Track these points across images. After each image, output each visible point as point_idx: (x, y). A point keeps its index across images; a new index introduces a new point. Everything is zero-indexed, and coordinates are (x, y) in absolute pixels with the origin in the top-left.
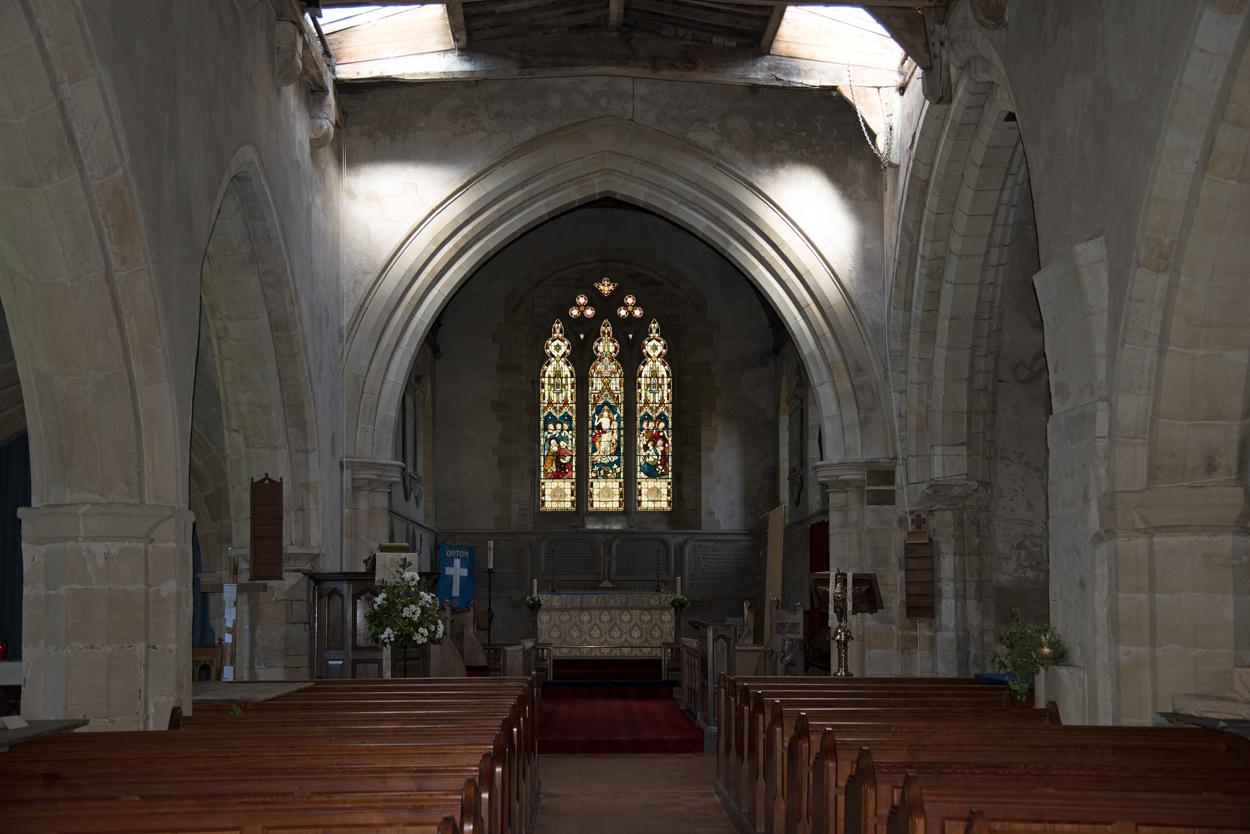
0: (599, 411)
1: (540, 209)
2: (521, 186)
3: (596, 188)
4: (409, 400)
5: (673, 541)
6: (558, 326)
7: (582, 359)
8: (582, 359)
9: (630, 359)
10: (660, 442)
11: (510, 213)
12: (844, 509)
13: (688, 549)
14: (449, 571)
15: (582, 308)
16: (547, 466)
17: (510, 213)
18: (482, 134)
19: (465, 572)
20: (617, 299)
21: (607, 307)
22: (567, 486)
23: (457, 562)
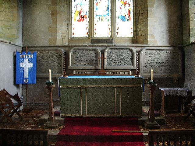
5: (135, 50)
10: (127, 5)
16: (75, 17)
23: (27, 60)
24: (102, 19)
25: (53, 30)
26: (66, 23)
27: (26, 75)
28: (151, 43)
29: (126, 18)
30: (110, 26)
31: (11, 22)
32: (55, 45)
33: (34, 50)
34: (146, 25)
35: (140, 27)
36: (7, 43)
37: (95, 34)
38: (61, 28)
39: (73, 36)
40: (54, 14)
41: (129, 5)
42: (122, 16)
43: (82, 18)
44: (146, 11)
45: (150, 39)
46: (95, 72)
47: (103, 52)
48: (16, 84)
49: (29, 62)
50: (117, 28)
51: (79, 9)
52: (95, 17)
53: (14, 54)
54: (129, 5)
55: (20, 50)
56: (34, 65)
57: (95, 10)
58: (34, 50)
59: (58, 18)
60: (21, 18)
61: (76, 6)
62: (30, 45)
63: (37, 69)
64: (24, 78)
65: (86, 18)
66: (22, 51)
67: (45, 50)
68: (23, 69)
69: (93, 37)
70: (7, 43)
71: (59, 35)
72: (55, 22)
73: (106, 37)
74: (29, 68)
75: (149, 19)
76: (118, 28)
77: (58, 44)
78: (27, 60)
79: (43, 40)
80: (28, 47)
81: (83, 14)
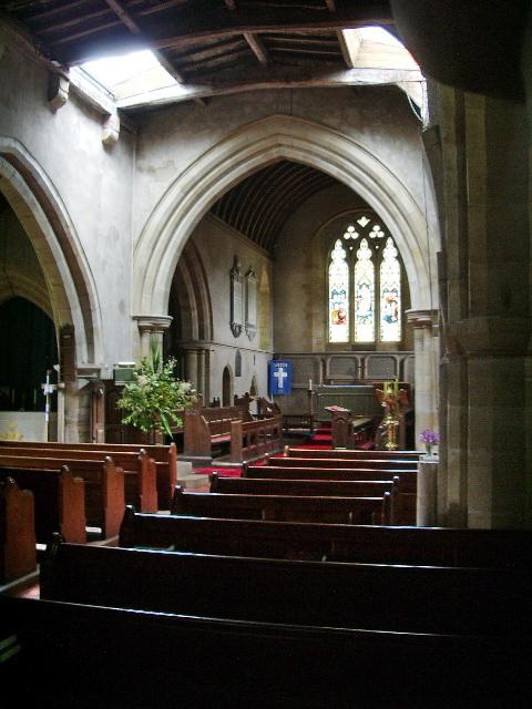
0: (361, 287)
1: (243, 169)
2: (230, 157)
3: (275, 154)
4: (186, 276)
5: (398, 359)
6: (339, 243)
7: (351, 260)
8: (351, 260)
9: (377, 259)
11: (226, 172)
12: (422, 340)
13: (366, 360)
14: (276, 374)
15: (351, 233)
16: (333, 318)
17: (226, 172)
18: (208, 131)
19: (286, 375)
20: (369, 228)
21: (364, 232)
22: (345, 327)
25: (308, 335)
26: (322, 325)
38: (317, 333)
40: (309, 316)
43: (341, 319)
46: (355, 382)
47: (363, 360)
71: (315, 341)
72: (310, 326)
77: (314, 352)
79: (297, 347)
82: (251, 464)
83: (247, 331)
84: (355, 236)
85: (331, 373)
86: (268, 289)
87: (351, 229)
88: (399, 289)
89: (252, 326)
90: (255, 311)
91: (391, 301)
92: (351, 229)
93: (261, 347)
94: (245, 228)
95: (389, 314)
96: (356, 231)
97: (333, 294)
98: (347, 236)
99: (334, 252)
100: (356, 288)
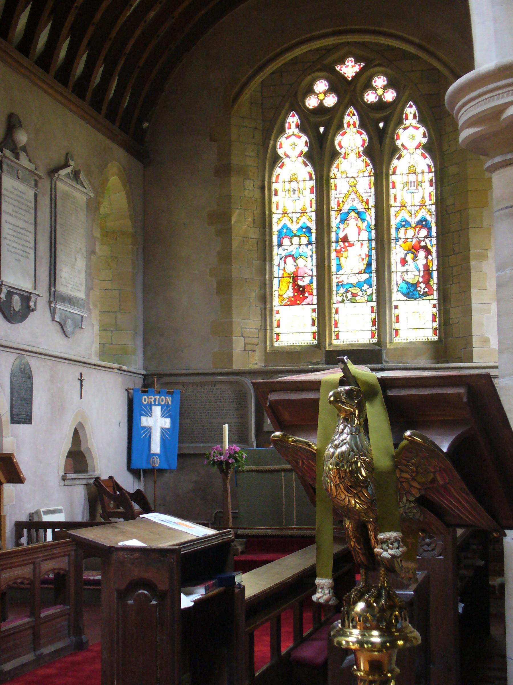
6: (293, 120)
10: (422, 254)
23: (157, 410)
24: (354, 295)
26: (256, 308)
27: (156, 447)
28: (480, 358)
29: (419, 289)
30: (374, 315)
31: (119, 316)
32: (227, 370)
33: (176, 384)
34: (468, 311)
35: (455, 313)
36: (113, 369)
37: (334, 337)
39: (276, 344)
41: (428, 252)
42: (407, 283)
44: (467, 270)
45: (477, 348)
48: (134, 472)
49: (163, 416)
50: (394, 319)
51: (290, 267)
52: (334, 288)
53: (129, 393)
54: (428, 252)
55: (139, 382)
56: (173, 423)
57: (334, 269)
58: (176, 384)
59: (234, 297)
60: (140, 301)
61: (283, 259)
62: (164, 369)
63: (182, 434)
64: (150, 455)
65: (311, 294)
66: (145, 386)
67: (203, 384)
68: (148, 430)
69: (331, 344)
70: (113, 369)
73: (365, 342)
74: (163, 431)
75: (474, 292)
76: (397, 317)
77: (236, 366)
78: (157, 410)
80: (161, 376)
81: (337, 169)
82: (352, 388)
83: (53, 312)
84: (331, 101)
85: (285, 525)
86: (128, 222)
87: (321, 86)
88: (432, 220)
89: (69, 300)
90: (81, 264)
91: (414, 249)
92: (321, 86)
93: (103, 354)
94: (244, 401)
95: (411, 278)
96: (332, 89)
97: (280, 237)
98: (312, 102)
99: (283, 140)
100: (334, 221)
